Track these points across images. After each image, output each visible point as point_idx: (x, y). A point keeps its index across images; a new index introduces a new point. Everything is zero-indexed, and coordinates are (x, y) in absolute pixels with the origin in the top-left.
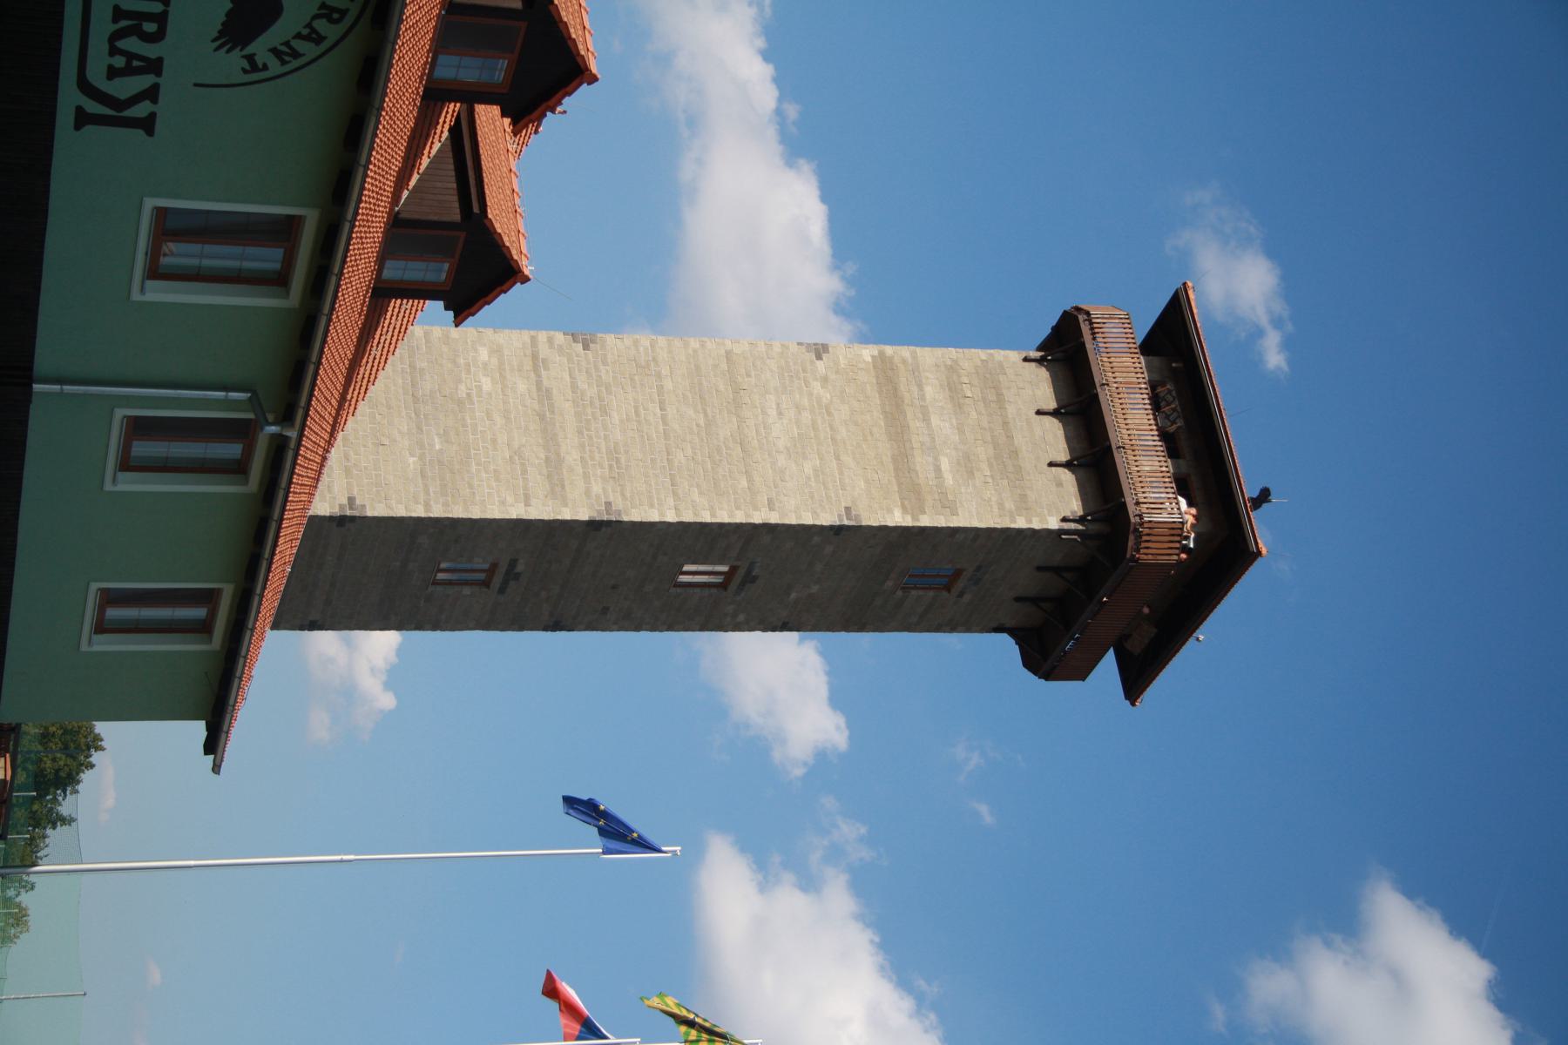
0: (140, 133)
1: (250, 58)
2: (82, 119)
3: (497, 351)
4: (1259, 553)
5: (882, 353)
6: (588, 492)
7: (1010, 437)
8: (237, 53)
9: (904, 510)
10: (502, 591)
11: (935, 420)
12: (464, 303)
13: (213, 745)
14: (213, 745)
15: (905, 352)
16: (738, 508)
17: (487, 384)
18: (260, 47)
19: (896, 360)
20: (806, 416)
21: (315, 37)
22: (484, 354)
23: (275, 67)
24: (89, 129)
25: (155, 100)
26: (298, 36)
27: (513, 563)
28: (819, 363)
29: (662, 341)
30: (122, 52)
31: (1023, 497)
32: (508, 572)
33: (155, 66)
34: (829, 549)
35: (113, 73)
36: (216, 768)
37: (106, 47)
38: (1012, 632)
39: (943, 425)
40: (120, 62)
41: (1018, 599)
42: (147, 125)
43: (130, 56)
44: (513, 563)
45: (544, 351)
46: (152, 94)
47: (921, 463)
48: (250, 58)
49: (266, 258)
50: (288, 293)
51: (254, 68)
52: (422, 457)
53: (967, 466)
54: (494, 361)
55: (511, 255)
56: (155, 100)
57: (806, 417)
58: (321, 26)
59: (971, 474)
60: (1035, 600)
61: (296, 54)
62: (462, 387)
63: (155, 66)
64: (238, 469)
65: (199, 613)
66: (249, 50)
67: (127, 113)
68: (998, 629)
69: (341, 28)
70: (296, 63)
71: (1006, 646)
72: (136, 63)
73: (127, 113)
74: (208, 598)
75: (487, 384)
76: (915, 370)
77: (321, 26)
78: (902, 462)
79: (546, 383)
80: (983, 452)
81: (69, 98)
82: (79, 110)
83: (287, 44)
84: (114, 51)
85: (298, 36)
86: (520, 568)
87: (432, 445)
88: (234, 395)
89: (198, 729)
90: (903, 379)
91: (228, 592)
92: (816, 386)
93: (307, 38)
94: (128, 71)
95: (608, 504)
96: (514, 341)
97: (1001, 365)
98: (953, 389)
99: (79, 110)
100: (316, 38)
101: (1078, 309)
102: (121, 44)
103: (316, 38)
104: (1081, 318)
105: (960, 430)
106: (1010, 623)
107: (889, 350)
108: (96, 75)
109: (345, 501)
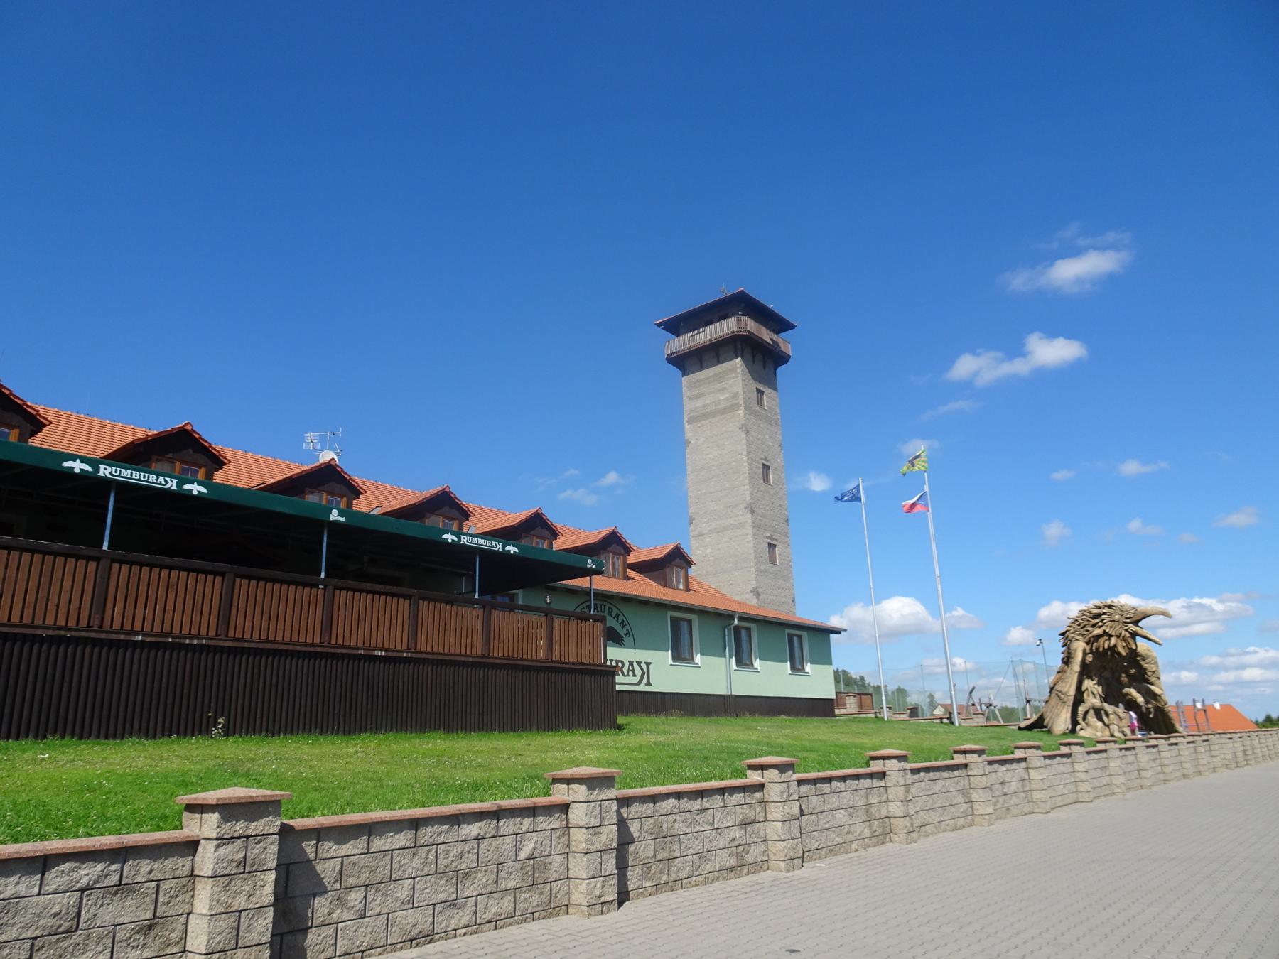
0: (650, 666)
1: (625, 635)
2: (648, 683)
3: (697, 548)
4: (789, 356)
5: (687, 422)
6: (741, 515)
7: (711, 377)
8: (624, 639)
9: (739, 409)
10: (777, 540)
11: (707, 402)
12: (688, 563)
13: (838, 632)
14: (838, 632)
15: (685, 415)
16: (742, 465)
17: (709, 551)
18: (622, 632)
19: (689, 416)
20: (710, 445)
21: (617, 616)
22: (699, 552)
23: (627, 627)
24: (651, 681)
25: (641, 662)
26: (617, 621)
27: (768, 538)
28: (692, 442)
29: (690, 494)
30: (628, 672)
31: (730, 370)
32: (770, 539)
33: (631, 663)
34: (754, 434)
35: (634, 675)
36: (845, 630)
37: (627, 677)
38: (775, 370)
39: (709, 400)
40: (631, 673)
41: (764, 368)
42: (648, 664)
43: (629, 670)
44: (768, 538)
45: (696, 533)
46: (639, 663)
47: (722, 406)
48: (625, 635)
49: (684, 626)
50: (671, 617)
51: (628, 633)
52: (735, 570)
53: (722, 390)
54: (702, 549)
55: (308, 470)
56: (641, 662)
57: (710, 445)
58: (614, 614)
59: (725, 388)
60: (754, 357)
61: (623, 621)
62: (711, 558)
63: (631, 663)
64: (749, 630)
65: (795, 639)
66: (623, 635)
67: (645, 670)
68: (775, 374)
69: (614, 608)
70: (625, 621)
71: (780, 370)
72: (631, 668)
73: (645, 670)
74: (790, 637)
75: (709, 551)
76: (692, 411)
77: (614, 614)
78: (723, 412)
79: (707, 532)
80: (718, 386)
81: (643, 688)
82: (646, 684)
83: (620, 624)
84: (628, 675)
85: (617, 621)
86: (769, 535)
87: (731, 567)
88: (727, 634)
89: (833, 637)
90: (696, 414)
91: (788, 631)
92: (700, 442)
93: (618, 618)
94: (633, 671)
95: (745, 508)
96: (694, 544)
97: (687, 382)
98: (696, 397)
99: (646, 684)
100: (618, 615)
101: (666, 359)
102: (626, 674)
103: (618, 615)
104: (1103, 712)
105: (709, 394)
106: (773, 370)
107: (686, 419)
108: (636, 680)
109: (752, 594)
